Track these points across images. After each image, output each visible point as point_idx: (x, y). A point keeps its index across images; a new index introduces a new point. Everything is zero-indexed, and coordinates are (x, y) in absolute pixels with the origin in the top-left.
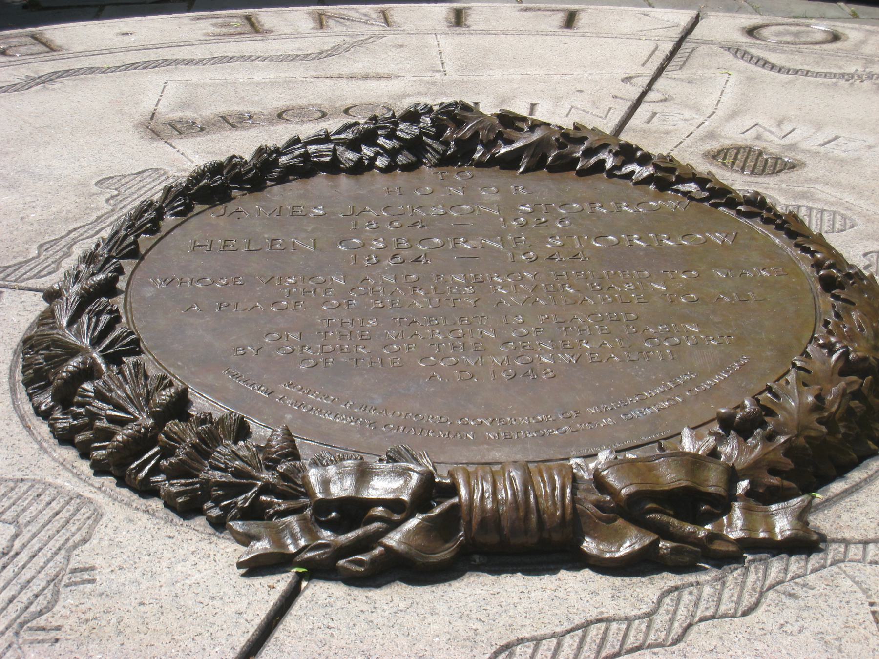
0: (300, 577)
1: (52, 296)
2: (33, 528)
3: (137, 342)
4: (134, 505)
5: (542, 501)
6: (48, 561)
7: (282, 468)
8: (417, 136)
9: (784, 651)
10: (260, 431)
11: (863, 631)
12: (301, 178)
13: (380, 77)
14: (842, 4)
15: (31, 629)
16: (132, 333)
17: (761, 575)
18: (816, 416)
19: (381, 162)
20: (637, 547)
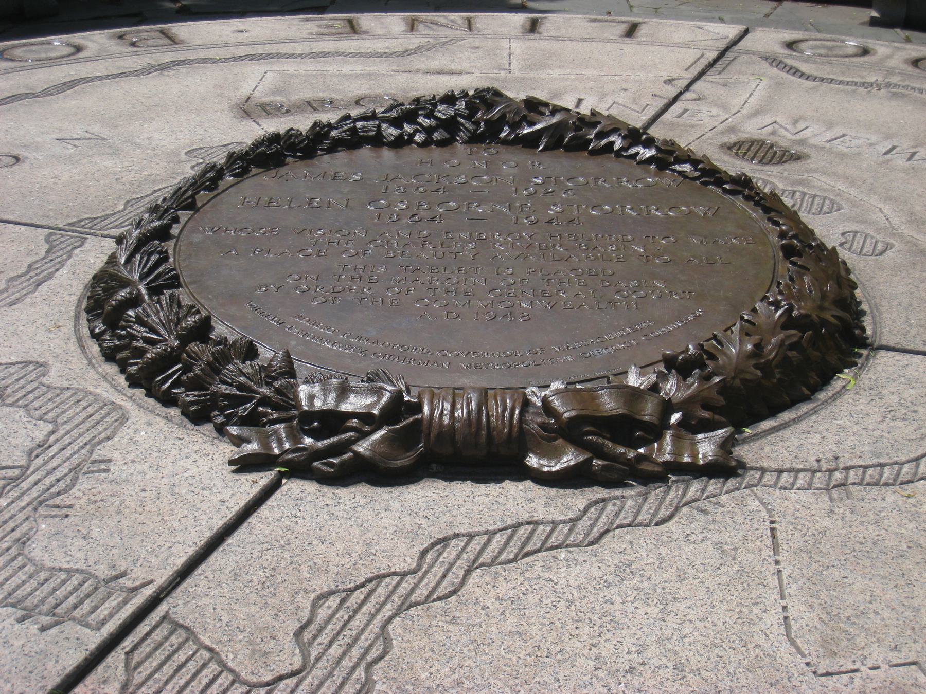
0: (282, 475)
1: (120, 240)
2: (68, 427)
3: (176, 277)
4: (157, 412)
5: (493, 420)
6: (74, 453)
7: (277, 384)
8: (451, 116)
9: (684, 556)
10: (266, 354)
11: (759, 544)
12: (348, 149)
13: (452, 73)
14: (898, 30)
15: (47, 506)
16: (174, 270)
17: (680, 493)
18: (753, 362)
19: (418, 138)
20: (572, 463)
